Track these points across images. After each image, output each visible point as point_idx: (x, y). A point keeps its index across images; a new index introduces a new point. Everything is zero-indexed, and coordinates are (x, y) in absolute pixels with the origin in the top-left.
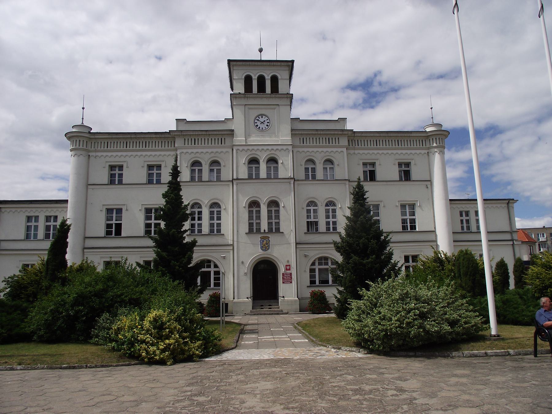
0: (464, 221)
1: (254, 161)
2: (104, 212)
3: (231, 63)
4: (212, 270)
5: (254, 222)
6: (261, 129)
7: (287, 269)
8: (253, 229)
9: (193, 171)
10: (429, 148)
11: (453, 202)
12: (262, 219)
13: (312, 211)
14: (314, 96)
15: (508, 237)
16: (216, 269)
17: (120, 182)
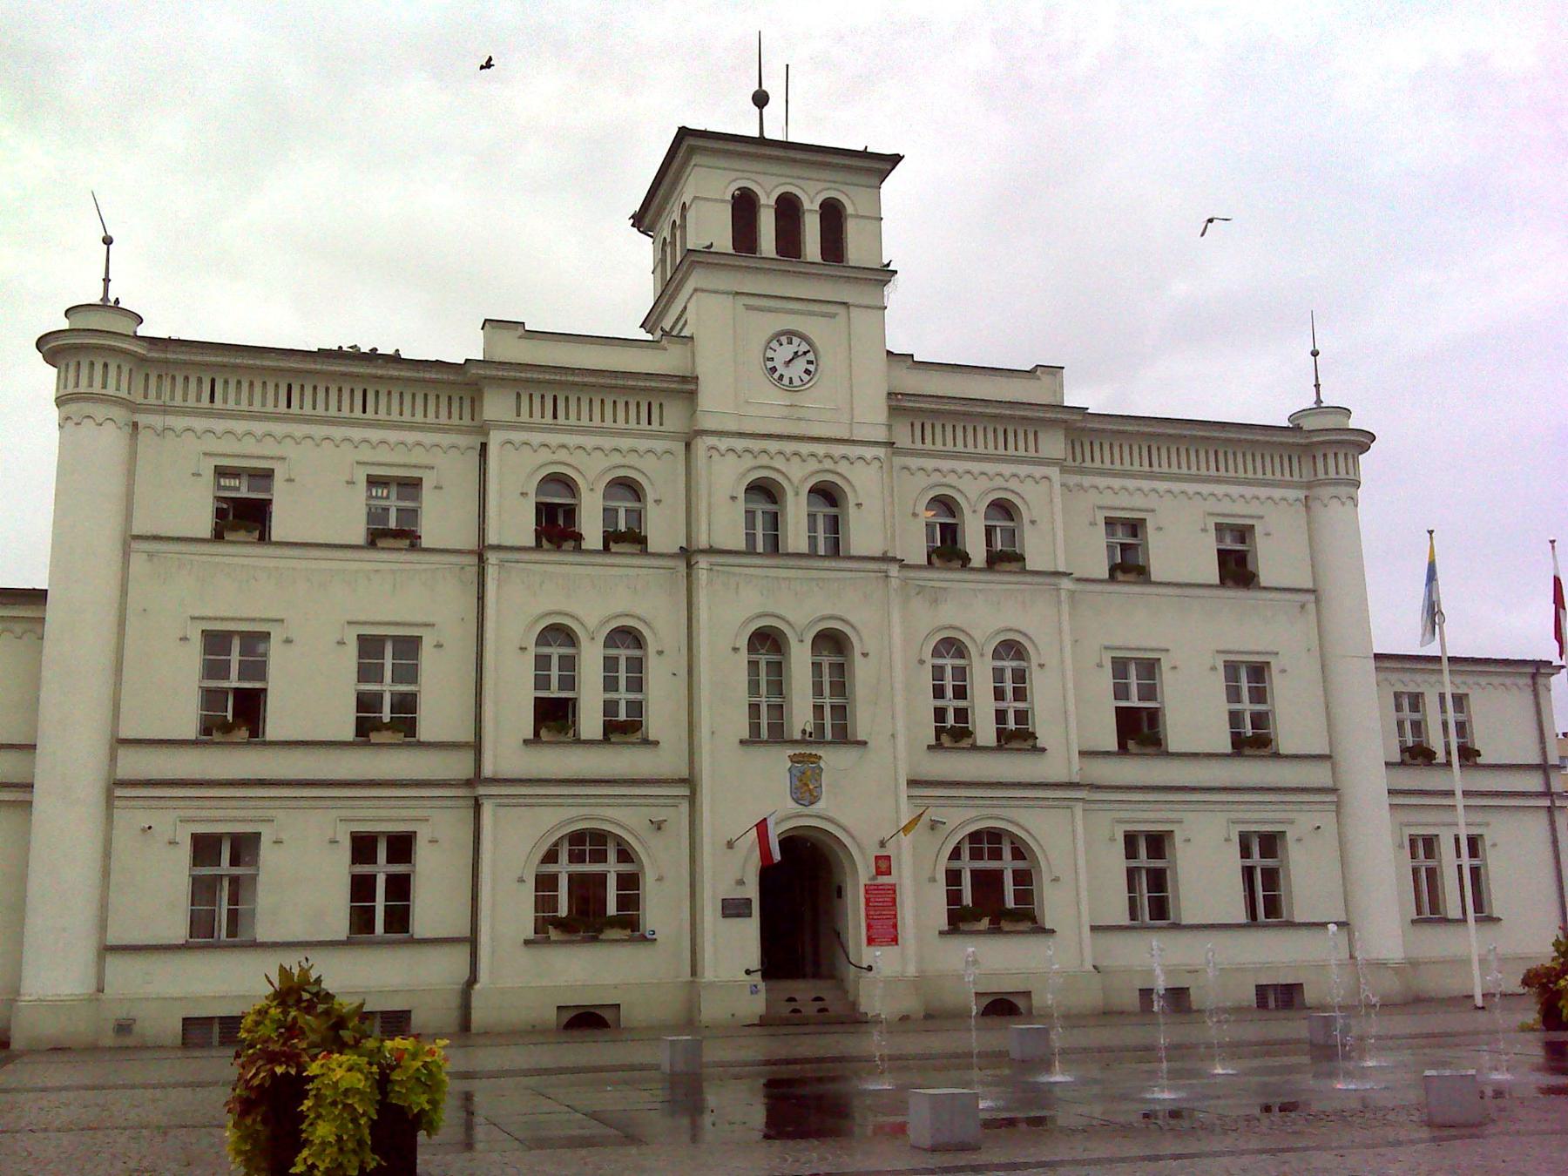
1: (764, 490)
2: (352, 648)
4: (612, 868)
5: (763, 702)
6: (786, 381)
7: (879, 872)
8: (767, 728)
10: (1309, 485)
11: (1387, 664)
13: (555, 662)
14: (951, 282)
15: (1534, 782)
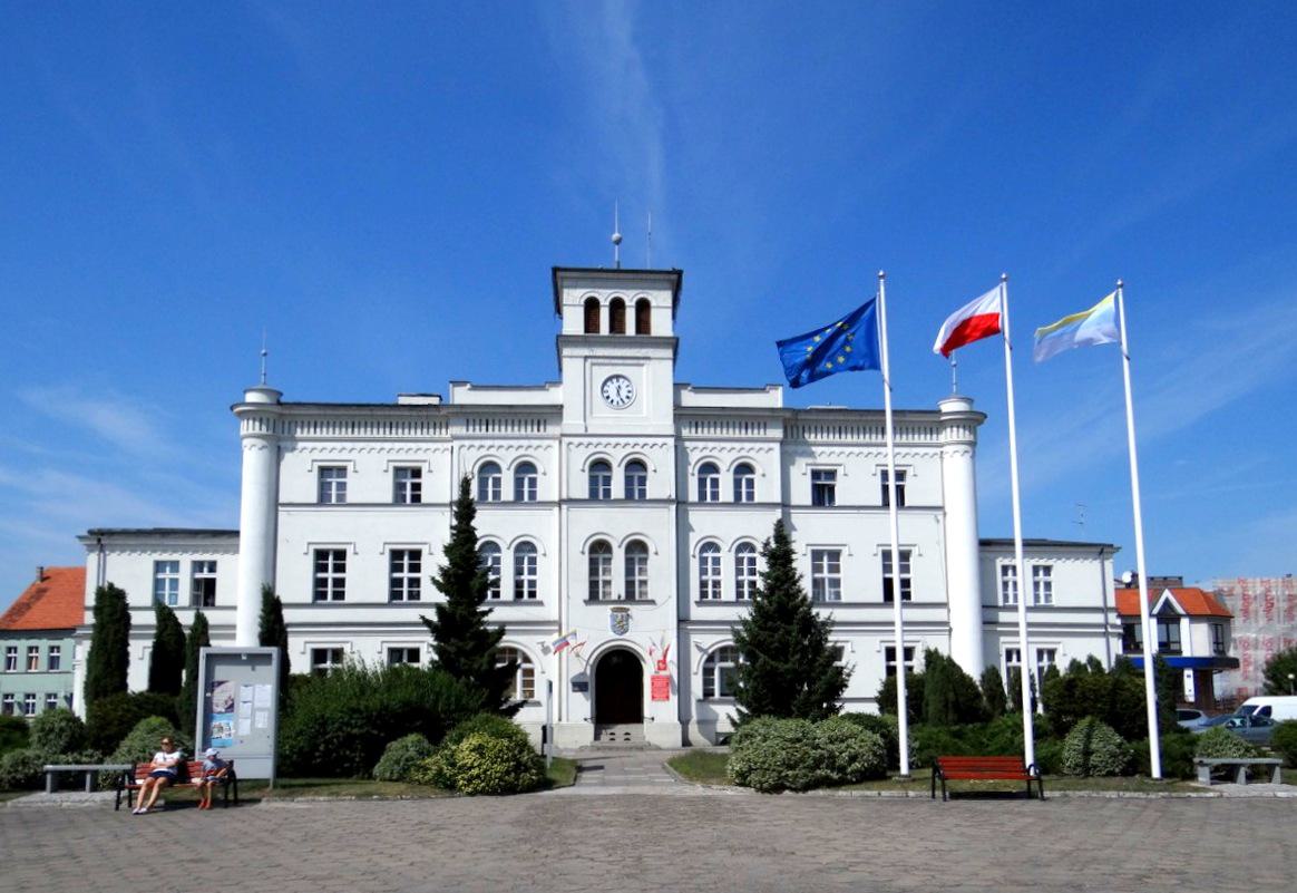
0: (1042, 585)
1: (600, 467)
2: (387, 556)
3: (559, 274)
6: (615, 403)
7: (659, 669)
12: (612, 570)
17: (416, 499)
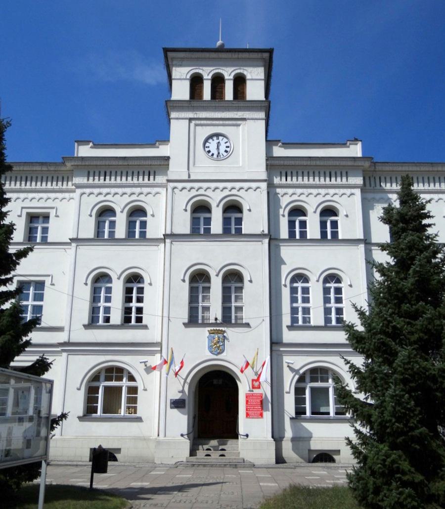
1: (201, 209)
7: (254, 387)
9: (323, 225)
16: (132, 384)
